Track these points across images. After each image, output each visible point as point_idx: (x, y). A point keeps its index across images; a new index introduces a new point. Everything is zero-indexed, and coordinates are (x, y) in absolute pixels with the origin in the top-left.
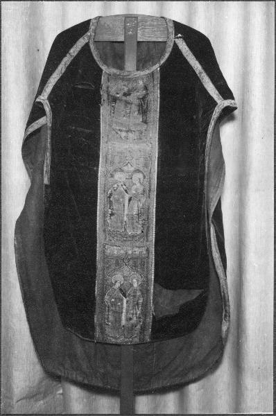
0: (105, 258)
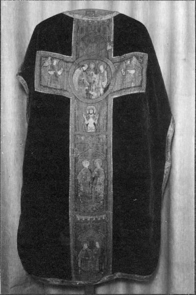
0: (77, 224)
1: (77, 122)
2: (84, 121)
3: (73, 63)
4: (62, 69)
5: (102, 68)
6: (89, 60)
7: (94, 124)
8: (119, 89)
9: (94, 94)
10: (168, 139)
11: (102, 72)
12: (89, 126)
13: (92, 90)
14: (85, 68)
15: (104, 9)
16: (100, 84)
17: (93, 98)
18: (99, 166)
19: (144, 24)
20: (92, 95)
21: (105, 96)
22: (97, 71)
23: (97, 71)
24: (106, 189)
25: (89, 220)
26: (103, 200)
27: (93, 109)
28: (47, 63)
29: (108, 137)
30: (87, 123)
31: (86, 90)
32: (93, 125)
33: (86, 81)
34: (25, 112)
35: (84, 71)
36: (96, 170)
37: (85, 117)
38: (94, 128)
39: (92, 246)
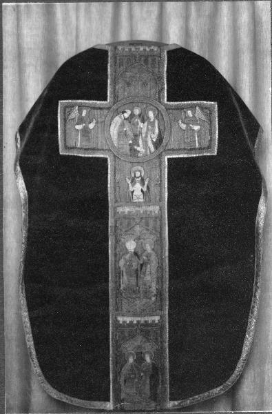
0: (117, 325)
1: (117, 190)
2: (128, 188)
3: (109, 108)
4: (94, 121)
5: (151, 114)
6: (132, 104)
7: (142, 191)
8: (177, 147)
9: (140, 149)
10: (258, 227)
11: (152, 120)
12: (134, 193)
13: (136, 148)
14: (126, 115)
15: (150, 40)
16: (149, 136)
17: (139, 155)
18: (148, 248)
19: (202, 55)
20: (139, 152)
21: (157, 153)
22: (143, 118)
23: (143, 118)
24: (160, 280)
25: (135, 322)
26: (156, 295)
27: (140, 171)
28: (75, 114)
29: (159, 209)
30: (132, 190)
31: (130, 145)
32: (141, 193)
33: (129, 133)
34: (21, 277)
35: (125, 119)
36: (145, 253)
37: (129, 182)
38: (142, 197)
39: (140, 359)
